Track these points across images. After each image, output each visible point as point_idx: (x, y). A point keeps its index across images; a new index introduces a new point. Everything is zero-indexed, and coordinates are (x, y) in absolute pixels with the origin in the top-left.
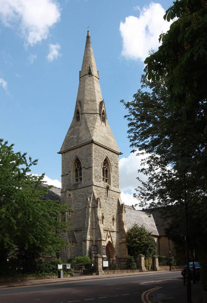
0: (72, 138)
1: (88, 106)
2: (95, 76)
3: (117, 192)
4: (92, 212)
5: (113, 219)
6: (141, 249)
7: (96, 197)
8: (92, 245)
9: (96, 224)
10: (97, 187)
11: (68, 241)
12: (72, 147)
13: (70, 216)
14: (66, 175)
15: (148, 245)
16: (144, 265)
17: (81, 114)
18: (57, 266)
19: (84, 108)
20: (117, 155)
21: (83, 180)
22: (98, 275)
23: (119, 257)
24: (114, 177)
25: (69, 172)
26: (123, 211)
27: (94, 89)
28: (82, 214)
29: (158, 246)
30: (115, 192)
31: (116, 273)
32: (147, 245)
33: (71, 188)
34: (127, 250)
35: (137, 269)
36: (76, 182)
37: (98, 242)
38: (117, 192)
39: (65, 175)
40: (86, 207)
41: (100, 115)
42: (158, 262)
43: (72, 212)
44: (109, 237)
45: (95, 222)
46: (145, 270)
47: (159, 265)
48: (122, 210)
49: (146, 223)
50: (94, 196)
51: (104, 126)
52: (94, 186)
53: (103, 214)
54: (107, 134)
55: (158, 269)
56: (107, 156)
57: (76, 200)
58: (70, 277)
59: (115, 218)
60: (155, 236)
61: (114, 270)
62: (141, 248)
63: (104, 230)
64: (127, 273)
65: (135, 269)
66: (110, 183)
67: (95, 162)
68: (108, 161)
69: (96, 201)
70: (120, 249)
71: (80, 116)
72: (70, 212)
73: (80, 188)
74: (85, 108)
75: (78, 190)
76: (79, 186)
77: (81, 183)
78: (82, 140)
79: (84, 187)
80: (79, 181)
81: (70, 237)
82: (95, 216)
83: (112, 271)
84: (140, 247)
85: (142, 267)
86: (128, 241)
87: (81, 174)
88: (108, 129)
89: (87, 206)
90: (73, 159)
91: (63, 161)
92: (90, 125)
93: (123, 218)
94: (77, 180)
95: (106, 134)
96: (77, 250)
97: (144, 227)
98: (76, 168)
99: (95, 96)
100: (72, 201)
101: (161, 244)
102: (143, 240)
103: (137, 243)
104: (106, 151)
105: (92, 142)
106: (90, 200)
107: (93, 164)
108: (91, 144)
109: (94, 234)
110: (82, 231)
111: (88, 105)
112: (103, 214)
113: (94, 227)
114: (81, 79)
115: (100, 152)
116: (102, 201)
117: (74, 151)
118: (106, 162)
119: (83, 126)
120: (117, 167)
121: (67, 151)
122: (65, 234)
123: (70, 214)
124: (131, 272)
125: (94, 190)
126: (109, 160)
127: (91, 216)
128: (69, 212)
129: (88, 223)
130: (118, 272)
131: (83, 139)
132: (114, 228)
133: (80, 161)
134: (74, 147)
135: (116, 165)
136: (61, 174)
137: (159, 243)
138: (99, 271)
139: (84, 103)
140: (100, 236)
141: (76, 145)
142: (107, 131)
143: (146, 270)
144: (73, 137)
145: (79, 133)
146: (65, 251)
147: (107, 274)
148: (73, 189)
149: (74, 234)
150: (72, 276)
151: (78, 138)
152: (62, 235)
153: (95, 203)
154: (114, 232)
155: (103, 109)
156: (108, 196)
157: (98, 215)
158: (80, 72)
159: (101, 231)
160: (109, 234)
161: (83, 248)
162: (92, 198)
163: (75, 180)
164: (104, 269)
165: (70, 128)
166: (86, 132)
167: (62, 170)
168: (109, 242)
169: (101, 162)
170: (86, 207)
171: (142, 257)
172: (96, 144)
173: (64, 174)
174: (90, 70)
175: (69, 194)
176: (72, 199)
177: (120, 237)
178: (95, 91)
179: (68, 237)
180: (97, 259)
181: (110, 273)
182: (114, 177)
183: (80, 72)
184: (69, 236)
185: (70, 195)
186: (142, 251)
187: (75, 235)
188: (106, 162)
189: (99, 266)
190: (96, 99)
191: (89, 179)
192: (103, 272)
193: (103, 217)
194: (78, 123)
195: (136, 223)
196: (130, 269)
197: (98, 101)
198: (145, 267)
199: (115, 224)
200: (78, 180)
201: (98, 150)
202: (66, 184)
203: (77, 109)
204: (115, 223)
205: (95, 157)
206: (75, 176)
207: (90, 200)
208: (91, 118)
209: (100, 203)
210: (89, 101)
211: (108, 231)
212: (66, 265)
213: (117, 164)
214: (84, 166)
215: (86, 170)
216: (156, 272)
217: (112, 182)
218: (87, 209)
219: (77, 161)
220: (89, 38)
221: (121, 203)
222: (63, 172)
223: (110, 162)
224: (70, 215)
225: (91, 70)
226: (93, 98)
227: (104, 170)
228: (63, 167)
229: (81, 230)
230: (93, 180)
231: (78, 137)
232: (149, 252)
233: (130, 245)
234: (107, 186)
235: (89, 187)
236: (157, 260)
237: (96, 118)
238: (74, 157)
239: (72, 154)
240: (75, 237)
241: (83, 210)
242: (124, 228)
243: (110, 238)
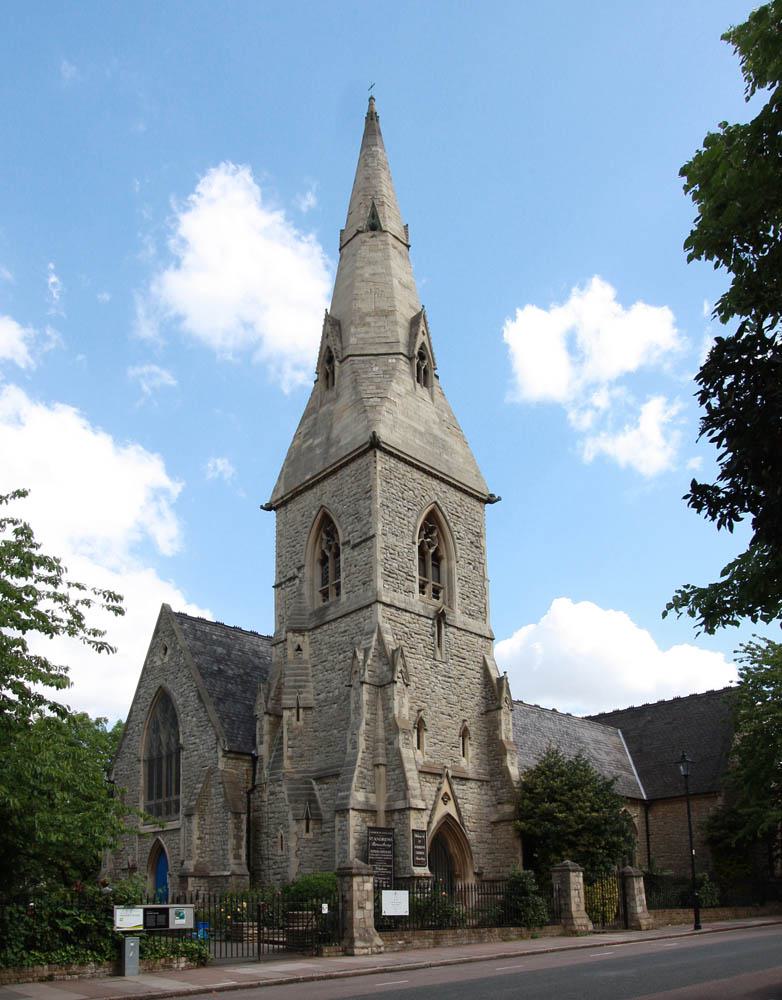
0: (310, 449)
1: (367, 332)
2: (394, 236)
3: (481, 636)
4: (372, 704)
5: (464, 734)
6: (572, 845)
7: (392, 647)
8: (369, 828)
9: (389, 747)
10: (393, 610)
11: (290, 817)
12: (308, 477)
13: (301, 723)
14: (290, 580)
15: (603, 828)
16: (583, 907)
17: (341, 362)
18: (111, 913)
19: (348, 340)
20: (476, 503)
21: (343, 591)
22: (353, 955)
23: (489, 874)
24: (466, 580)
26: (504, 704)
27: (390, 275)
28: (339, 715)
29: (645, 837)
30: (471, 633)
31: (450, 943)
32: (597, 826)
33: (303, 623)
34: (520, 848)
35: (553, 923)
36: (324, 601)
37: (396, 816)
38: (481, 636)
39: (285, 582)
41: (410, 359)
42: (644, 896)
43: (305, 708)
44: (446, 799)
45: (387, 739)
46: (586, 926)
47: (650, 906)
48: (500, 700)
49: (596, 754)
50: (381, 641)
51: (427, 398)
52: (380, 607)
53: (419, 711)
54: (435, 427)
55: (644, 922)
56: (436, 502)
57: (320, 667)
58: (188, 968)
59: (472, 729)
60: (635, 801)
61: (441, 932)
62: (574, 839)
63: (420, 772)
64: (505, 940)
65: (543, 924)
66: (450, 601)
67: (387, 517)
68: (443, 521)
69: (389, 659)
70: (493, 843)
71: (336, 368)
72: (301, 711)
73: (335, 620)
74: (353, 340)
75: (325, 627)
76: (332, 614)
77: (339, 600)
78: (341, 448)
79: (344, 616)
80: (332, 598)
81: (296, 801)
82: (386, 718)
83: (427, 937)
84: (571, 837)
85: (575, 915)
86: (521, 814)
88: (442, 411)
89: (355, 682)
90: (312, 520)
91: (279, 534)
92: (368, 389)
93: (503, 727)
94: (325, 594)
95: (433, 426)
96: (324, 851)
97: (587, 762)
98: (323, 553)
99: (391, 298)
100: (307, 668)
101: (653, 829)
102: (581, 808)
103: (555, 821)
104: (435, 483)
105: (375, 444)
106: (366, 656)
107: (380, 526)
108: (372, 453)
109: (383, 785)
111: (364, 329)
112: (419, 711)
113: (381, 760)
114: (345, 250)
115: (410, 485)
116: (416, 662)
117: (315, 490)
118: (433, 524)
119: (346, 397)
120: (477, 547)
121: (292, 498)
122: (278, 788)
123: (301, 716)
124: (521, 937)
125: (380, 619)
126: (445, 517)
127: (368, 716)
128: (294, 711)
129: (355, 746)
130: (458, 937)
131: (342, 443)
132: (469, 764)
133: (335, 526)
135: (474, 539)
137: (647, 826)
138: (356, 935)
139: (352, 323)
140: (401, 794)
141: (319, 467)
142: (439, 416)
143: (591, 927)
145: (332, 425)
146: (280, 851)
147: (403, 949)
148: (311, 626)
150: (201, 961)
151: (329, 442)
152: (272, 794)
153: (385, 668)
154: (467, 779)
155: (421, 339)
156: (444, 649)
157: (396, 712)
158: (342, 231)
159: (408, 775)
160: (445, 788)
161: (338, 839)
162: (372, 650)
163: (319, 596)
164: (386, 925)
165: (304, 418)
166: (355, 414)
167: (278, 566)
168: (448, 815)
169: (412, 520)
171: (574, 871)
172: (390, 454)
173: (283, 580)
174: (374, 215)
175: (296, 646)
176: (306, 662)
177: (494, 799)
178: (391, 281)
179: (290, 802)
180: (347, 879)
181: (416, 943)
182: (466, 580)
183: (342, 231)
184: (294, 799)
185: (299, 649)
186: (579, 852)
187: (315, 796)
188: (433, 524)
189: (358, 915)
190: (394, 306)
191: (364, 584)
192: (378, 941)
193: (420, 725)
194: (331, 394)
195: (554, 746)
196: (515, 925)
197: (404, 314)
198: (585, 914)
199: (471, 751)
200: (327, 593)
201: (400, 476)
203: (328, 347)
204: (470, 748)
205: (386, 502)
206: (318, 580)
207: (366, 656)
208: (375, 369)
209: (405, 666)
210: (368, 314)
211: (440, 775)
212: (166, 911)
213: (479, 535)
214: (347, 539)
216: (633, 936)
217: (457, 599)
218: (353, 693)
219: (326, 525)
220: (372, 119)
221: (494, 675)
222: (279, 573)
223: (452, 524)
224: (298, 720)
225: (380, 216)
226: (384, 305)
227: (427, 553)
228: (279, 556)
229: (337, 775)
230: (380, 583)
231: (328, 439)
232: (608, 855)
233: (530, 829)
234: (437, 612)
236: (639, 885)
237: (394, 369)
238: (314, 513)
240: (316, 802)
241: (343, 698)
242: (509, 765)
243: (451, 803)
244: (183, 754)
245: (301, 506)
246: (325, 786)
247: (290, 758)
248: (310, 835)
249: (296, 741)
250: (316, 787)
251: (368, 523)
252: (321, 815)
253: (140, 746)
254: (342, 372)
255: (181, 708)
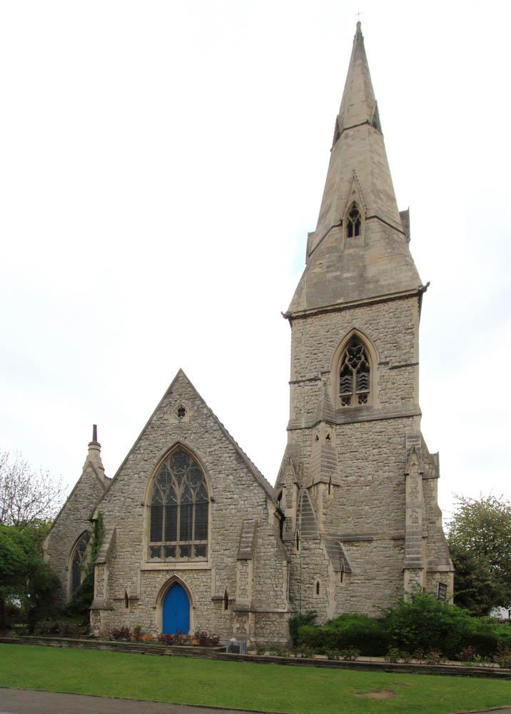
13: (331, 496)
25: (322, 374)
40: (408, 474)
72: (332, 486)
76: (365, 415)
78: (383, 286)
80: (354, 403)
87: (364, 384)
100: (335, 460)
110: (374, 544)
121: (316, 314)
134: (346, 303)
136: (287, 377)
144: (340, 276)
146: (315, 595)
149: (341, 549)
170: (408, 474)
185: (328, 438)
191: (402, 399)
202: (307, 407)
215: (394, 372)
219: (355, 353)
235: (405, 420)
239: (339, 326)
244: (212, 508)
245: (326, 323)
246: (355, 548)
247: (325, 523)
248: (343, 585)
249: (328, 510)
250: (343, 548)
251: (408, 352)
252: (350, 570)
253: (142, 491)
254: (367, 229)
255: (209, 466)
